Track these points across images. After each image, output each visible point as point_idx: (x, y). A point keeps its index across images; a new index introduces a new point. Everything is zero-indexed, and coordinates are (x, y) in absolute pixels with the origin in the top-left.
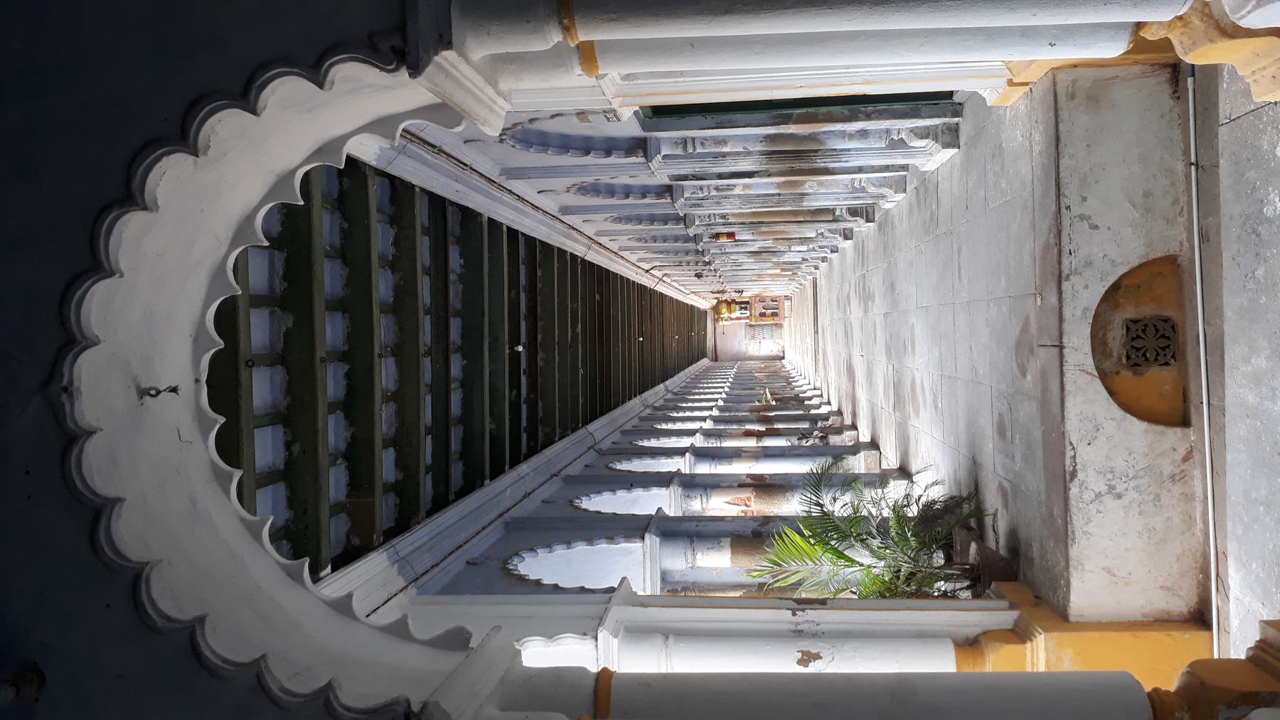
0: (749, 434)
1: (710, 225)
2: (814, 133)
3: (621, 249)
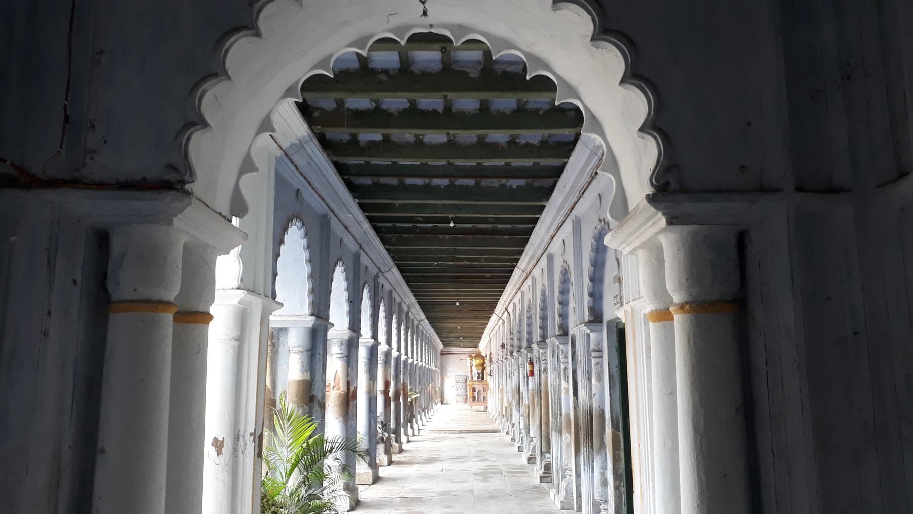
0: (387, 384)
1: (539, 360)
2: (605, 446)
3: (523, 293)
